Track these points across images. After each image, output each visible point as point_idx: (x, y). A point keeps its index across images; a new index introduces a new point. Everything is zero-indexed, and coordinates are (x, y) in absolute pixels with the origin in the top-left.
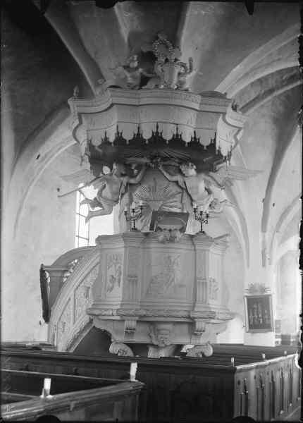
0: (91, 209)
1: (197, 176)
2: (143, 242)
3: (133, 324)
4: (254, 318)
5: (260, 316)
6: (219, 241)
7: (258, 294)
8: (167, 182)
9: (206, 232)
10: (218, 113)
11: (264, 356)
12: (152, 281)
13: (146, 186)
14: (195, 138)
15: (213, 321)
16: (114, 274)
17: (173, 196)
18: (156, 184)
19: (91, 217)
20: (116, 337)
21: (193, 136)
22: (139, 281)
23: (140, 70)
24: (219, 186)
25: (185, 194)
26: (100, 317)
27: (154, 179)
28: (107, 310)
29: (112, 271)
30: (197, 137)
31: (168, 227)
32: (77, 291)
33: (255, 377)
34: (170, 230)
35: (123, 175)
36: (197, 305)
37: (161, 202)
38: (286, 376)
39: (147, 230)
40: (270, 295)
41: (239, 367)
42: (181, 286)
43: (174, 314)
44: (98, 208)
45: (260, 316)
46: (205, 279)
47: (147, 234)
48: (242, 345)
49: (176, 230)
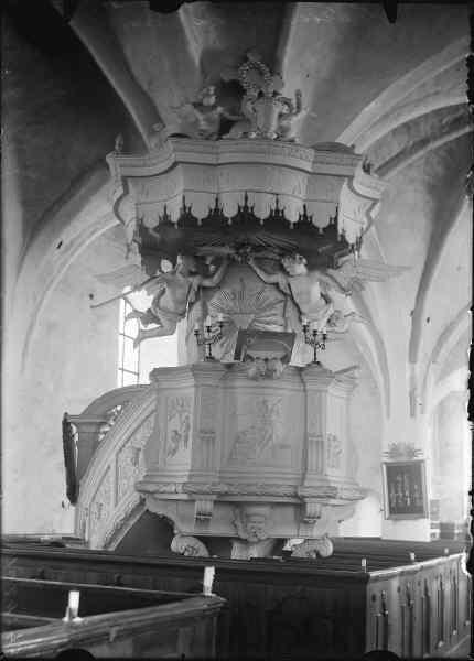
0: (142, 327)
1: (308, 275)
2: (224, 378)
3: (209, 506)
4: (398, 497)
5: (407, 493)
6: (343, 377)
7: (404, 459)
8: (261, 284)
9: (322, 362)
10: (341, 177)
11: (413, 556)
12: (238, 440)
13: (228, 291)
14: (305, 215)
15: (333, 501)
16: (178, 429)
17: (271, 306)
18: (244, 287)
19: (142, 339)
20: (182, 527)
21: (302, 213)
22: (218, 440)
23: (220, 109)
24: (343, 290)
25: (289, 303)
26: (157, 496)
27: (241, 280)
28: (167, 484)
29: (175, 424)
30: (309, 214)
31: (263, 354)
32: (120, 455)
33: (399, 590)
34: (266, 360)
35: (192, 274)
36: (308, 476)
37: (252, 316)
38: (448, 587)
39: (230, 359)
40: (422, 461)
41: (373, 574)
42: (283, 447)
43: (272, 490)
44: (153, 326)
45: (407, 493)
46: (321, 436)
47: (229, 366)
48: (378, 539)
49: (275, 359)
